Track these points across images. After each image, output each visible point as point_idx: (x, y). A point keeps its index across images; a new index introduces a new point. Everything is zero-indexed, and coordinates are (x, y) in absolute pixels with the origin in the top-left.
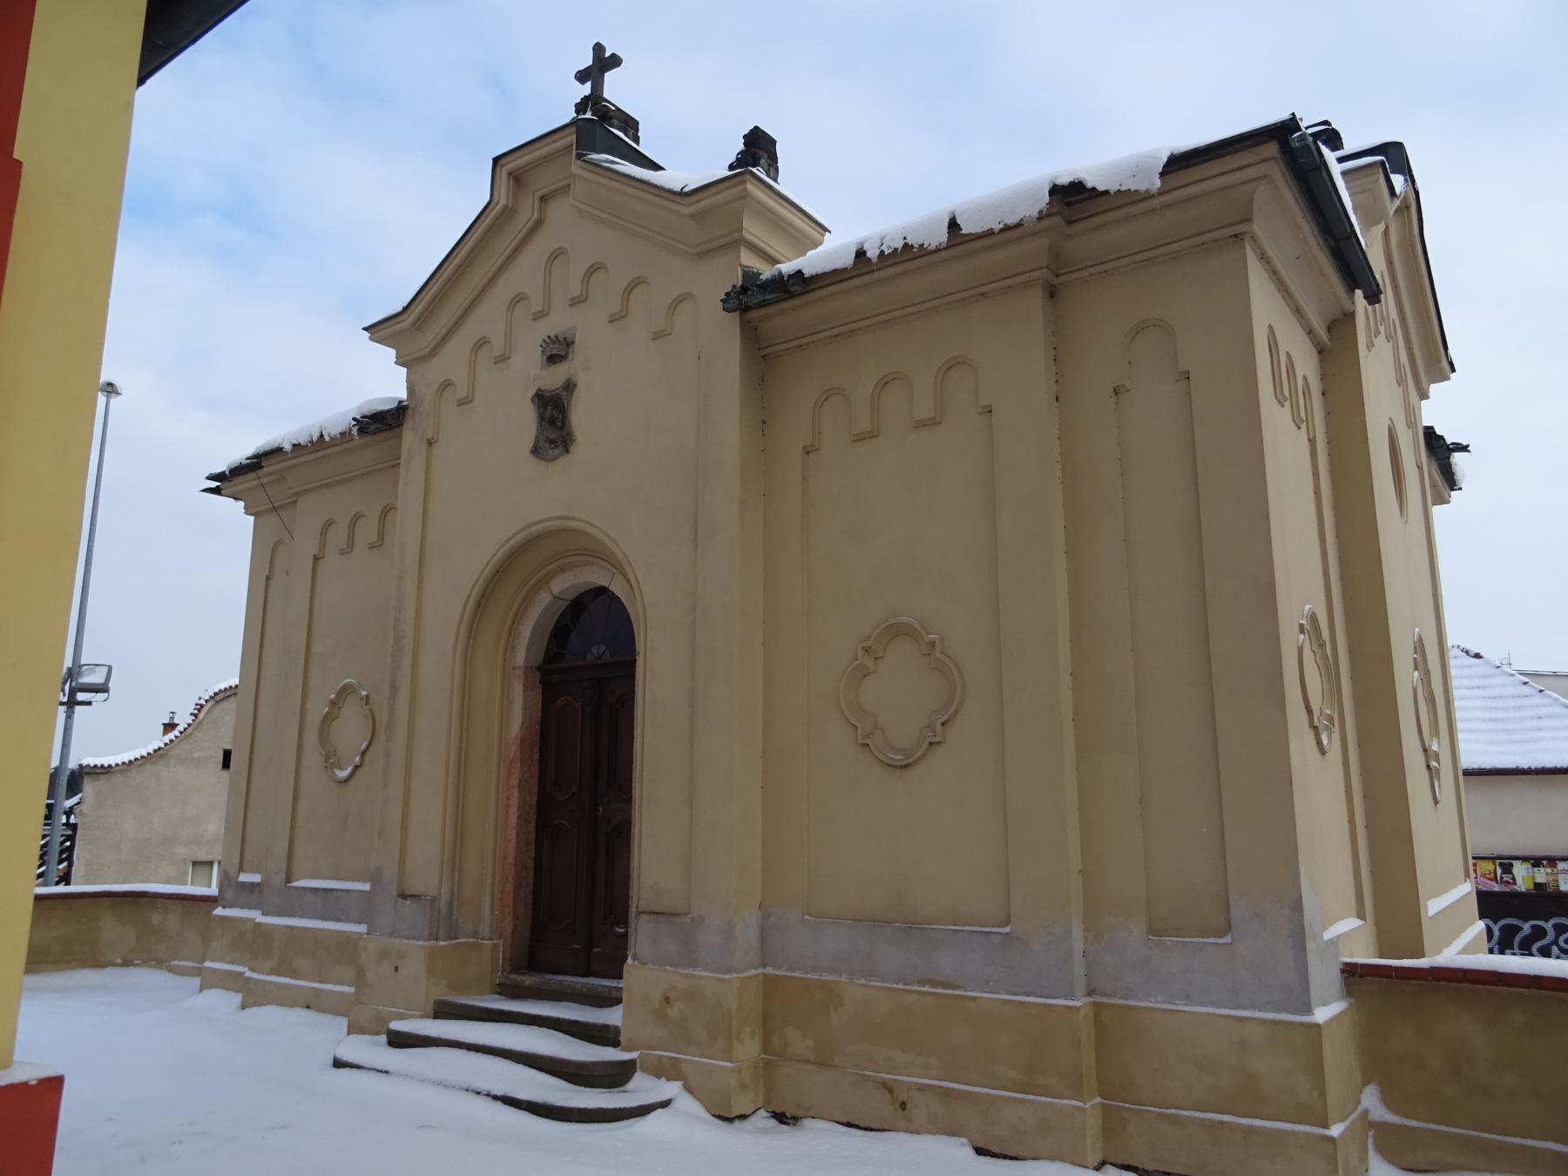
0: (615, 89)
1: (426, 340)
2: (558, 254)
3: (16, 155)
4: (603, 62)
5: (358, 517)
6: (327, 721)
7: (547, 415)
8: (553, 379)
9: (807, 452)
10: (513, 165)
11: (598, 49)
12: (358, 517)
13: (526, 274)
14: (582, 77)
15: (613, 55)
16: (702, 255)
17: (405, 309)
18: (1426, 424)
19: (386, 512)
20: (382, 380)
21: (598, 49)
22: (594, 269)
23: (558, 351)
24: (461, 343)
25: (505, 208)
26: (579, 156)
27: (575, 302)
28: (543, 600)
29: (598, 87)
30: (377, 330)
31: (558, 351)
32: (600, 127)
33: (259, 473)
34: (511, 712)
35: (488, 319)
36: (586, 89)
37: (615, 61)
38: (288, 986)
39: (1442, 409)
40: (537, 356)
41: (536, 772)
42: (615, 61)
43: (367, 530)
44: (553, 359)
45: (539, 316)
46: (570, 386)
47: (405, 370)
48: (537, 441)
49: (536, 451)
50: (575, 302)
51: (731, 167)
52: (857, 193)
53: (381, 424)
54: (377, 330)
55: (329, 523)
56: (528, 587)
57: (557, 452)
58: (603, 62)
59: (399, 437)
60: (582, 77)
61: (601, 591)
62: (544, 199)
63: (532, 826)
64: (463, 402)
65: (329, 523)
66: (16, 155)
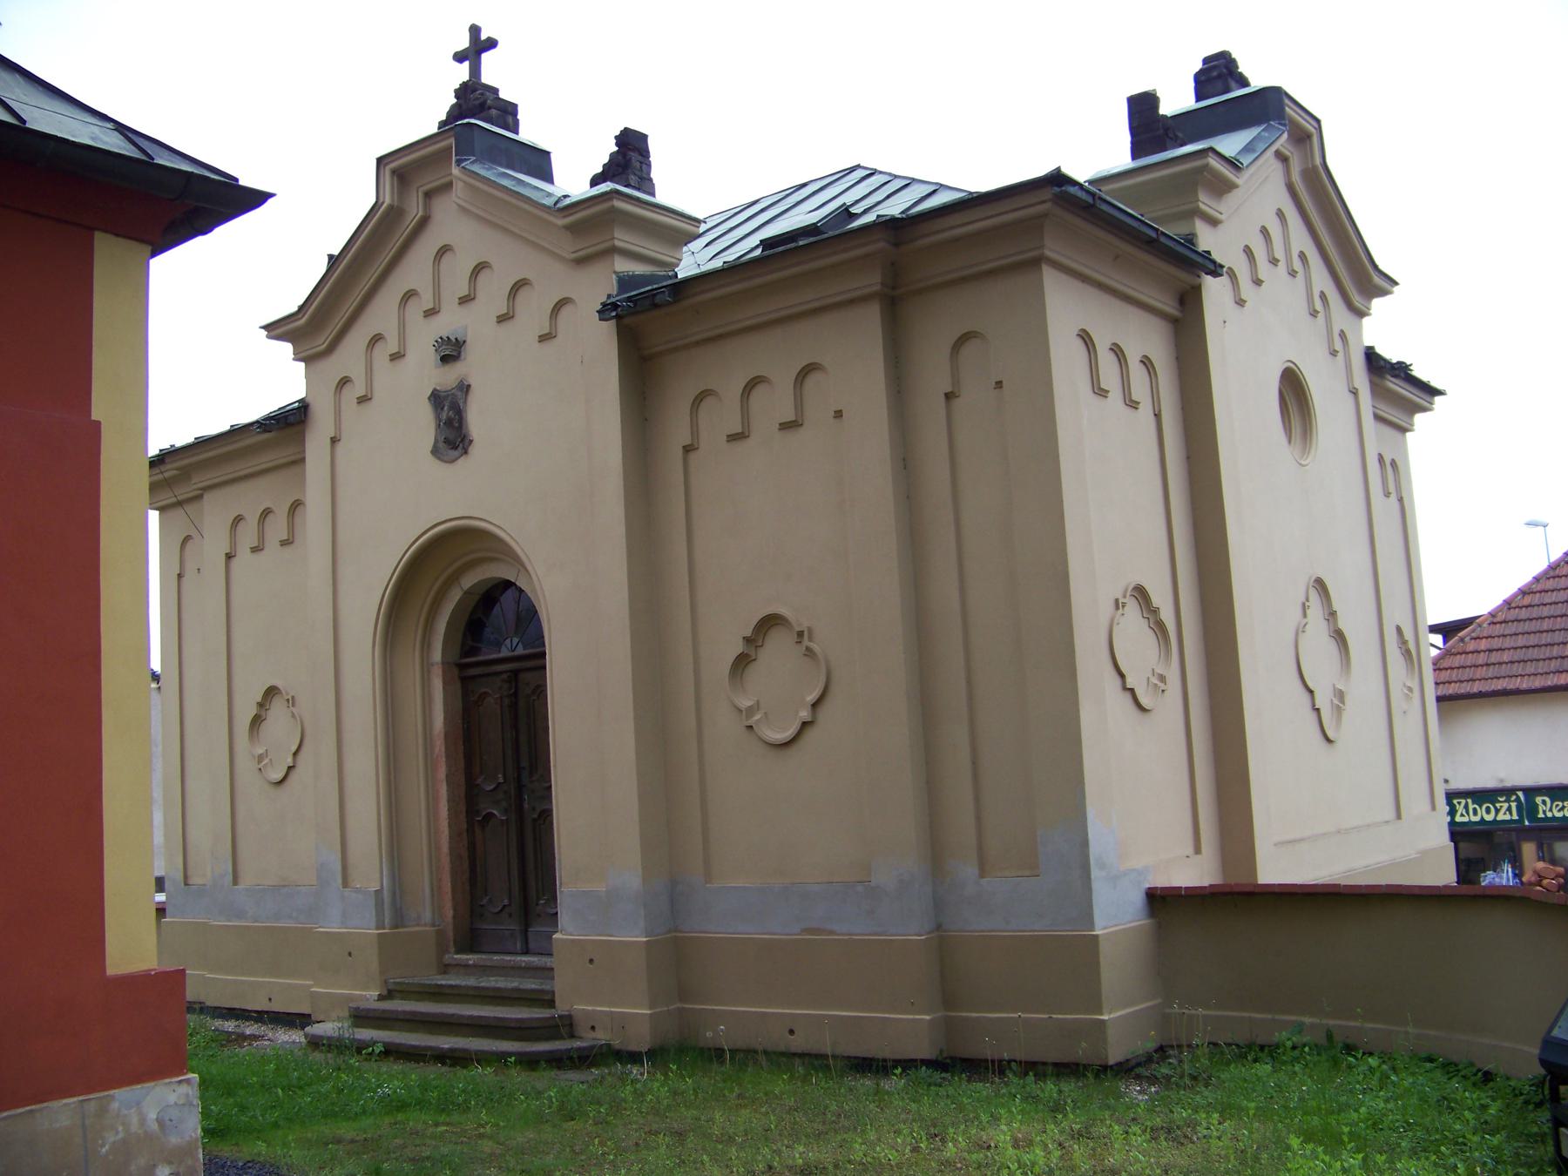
0: (493, 70)
1: (321, 342)
2: (444, 250)
3: (94, 417)
4: (478, 47)
5: (266, 513)
6: (257, 721)
7: (444, 416)
8: (447, 378)
9: (688, 450)
10: (393, 165)
11: (475, 30)
12: (266, 513)
13: (415, 272)
14: (459, 57)
15: (489, 39)
16: (581, 262)
17: (301, 308)
18: (1367, 343)
19: (296, 505)
20: (280, 380)
21: (475, 30)
22: (480, 268)
23: (451, 351)
24: (356, 340)
25: (391, 207)
26: (459, 162)
27: (465, 300)
28: (455, 596)
29: (475, 71)
30: (275, 330)
31: (451, 351)
32: (480, 115)
33: (163, 468)
34: (432, 707)
35: (382, 315)
36: (462, 72)
37: (491, 44)
38: (243, 974)
39: (1386, 329)
40: (431, 357)
41: (462, 764)
42: (491, 44)
43: (277, 528)
44: (445, 359)
45: (430, 313)
46: (465, 388)
47: (302, 365)
48: (436, 441)
49: (435, 452)
50: (465, 300)
51: (595, 181)
52: (725, 178)
53: (288, 424)
54: (275, 330)
55: (238, 519)
56: (435, 588)
57: (456, 453)
58: (478, 47)
59: (301, 441)
60: (459, 57)
61: (508, 584)
62: (428, 195)
63: (463, 816)
64: (363, 400)
65: (238, 519)
66: (94, 417)
